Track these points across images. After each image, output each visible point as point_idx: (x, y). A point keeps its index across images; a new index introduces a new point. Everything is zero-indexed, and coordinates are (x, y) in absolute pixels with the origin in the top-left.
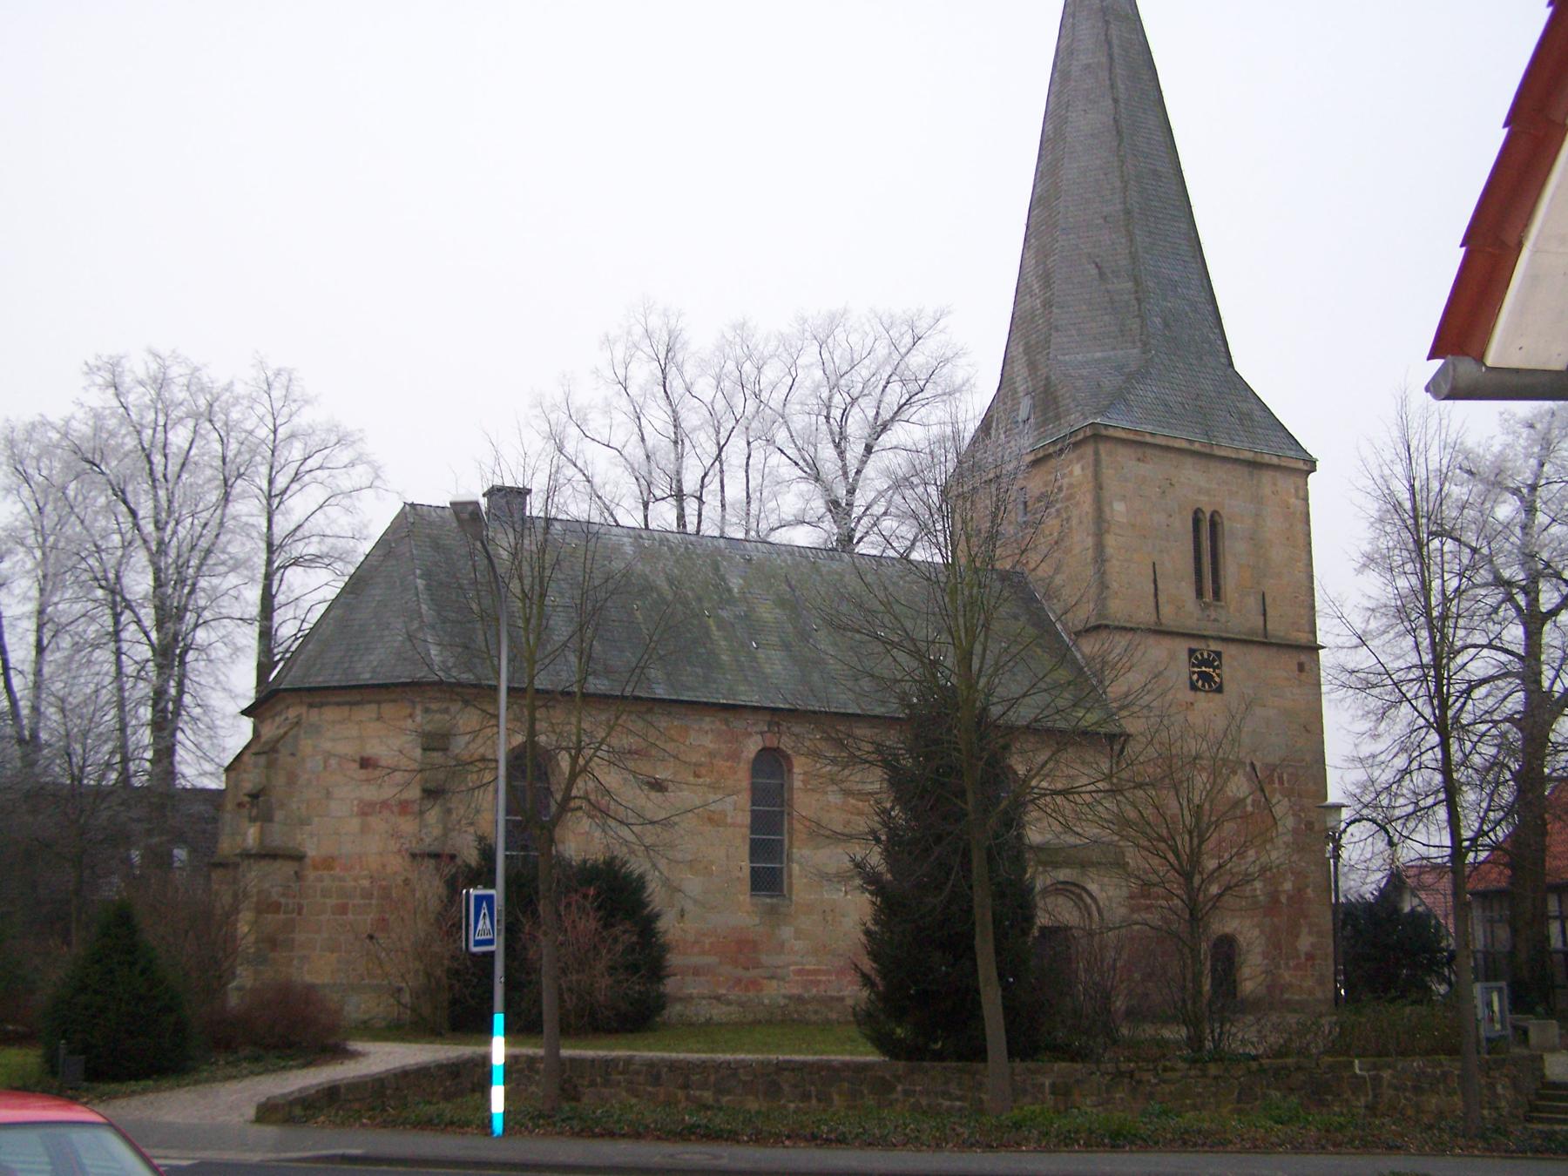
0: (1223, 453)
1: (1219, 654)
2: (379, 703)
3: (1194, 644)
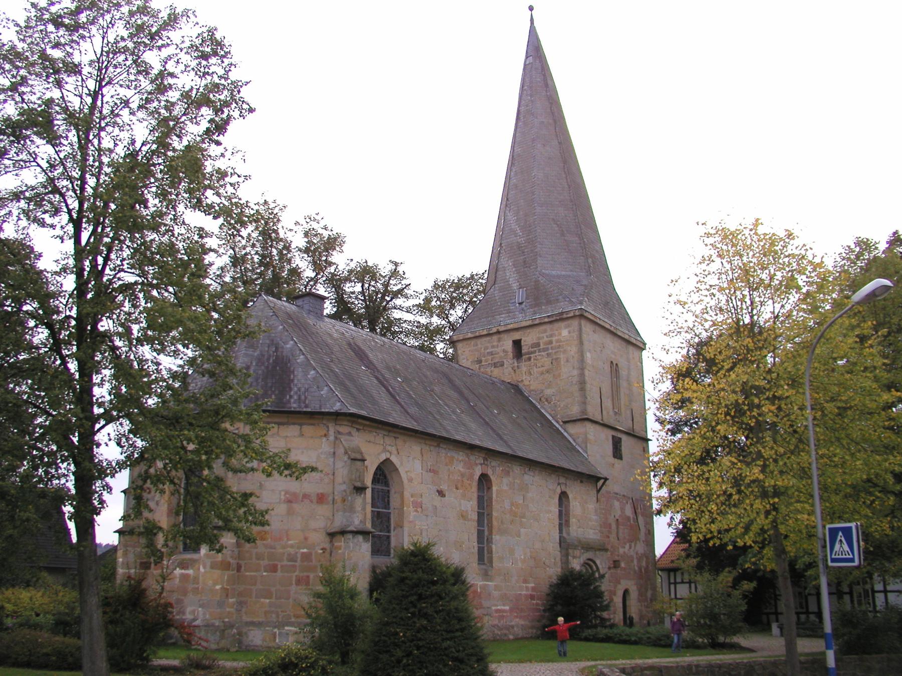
2: (301, 425)
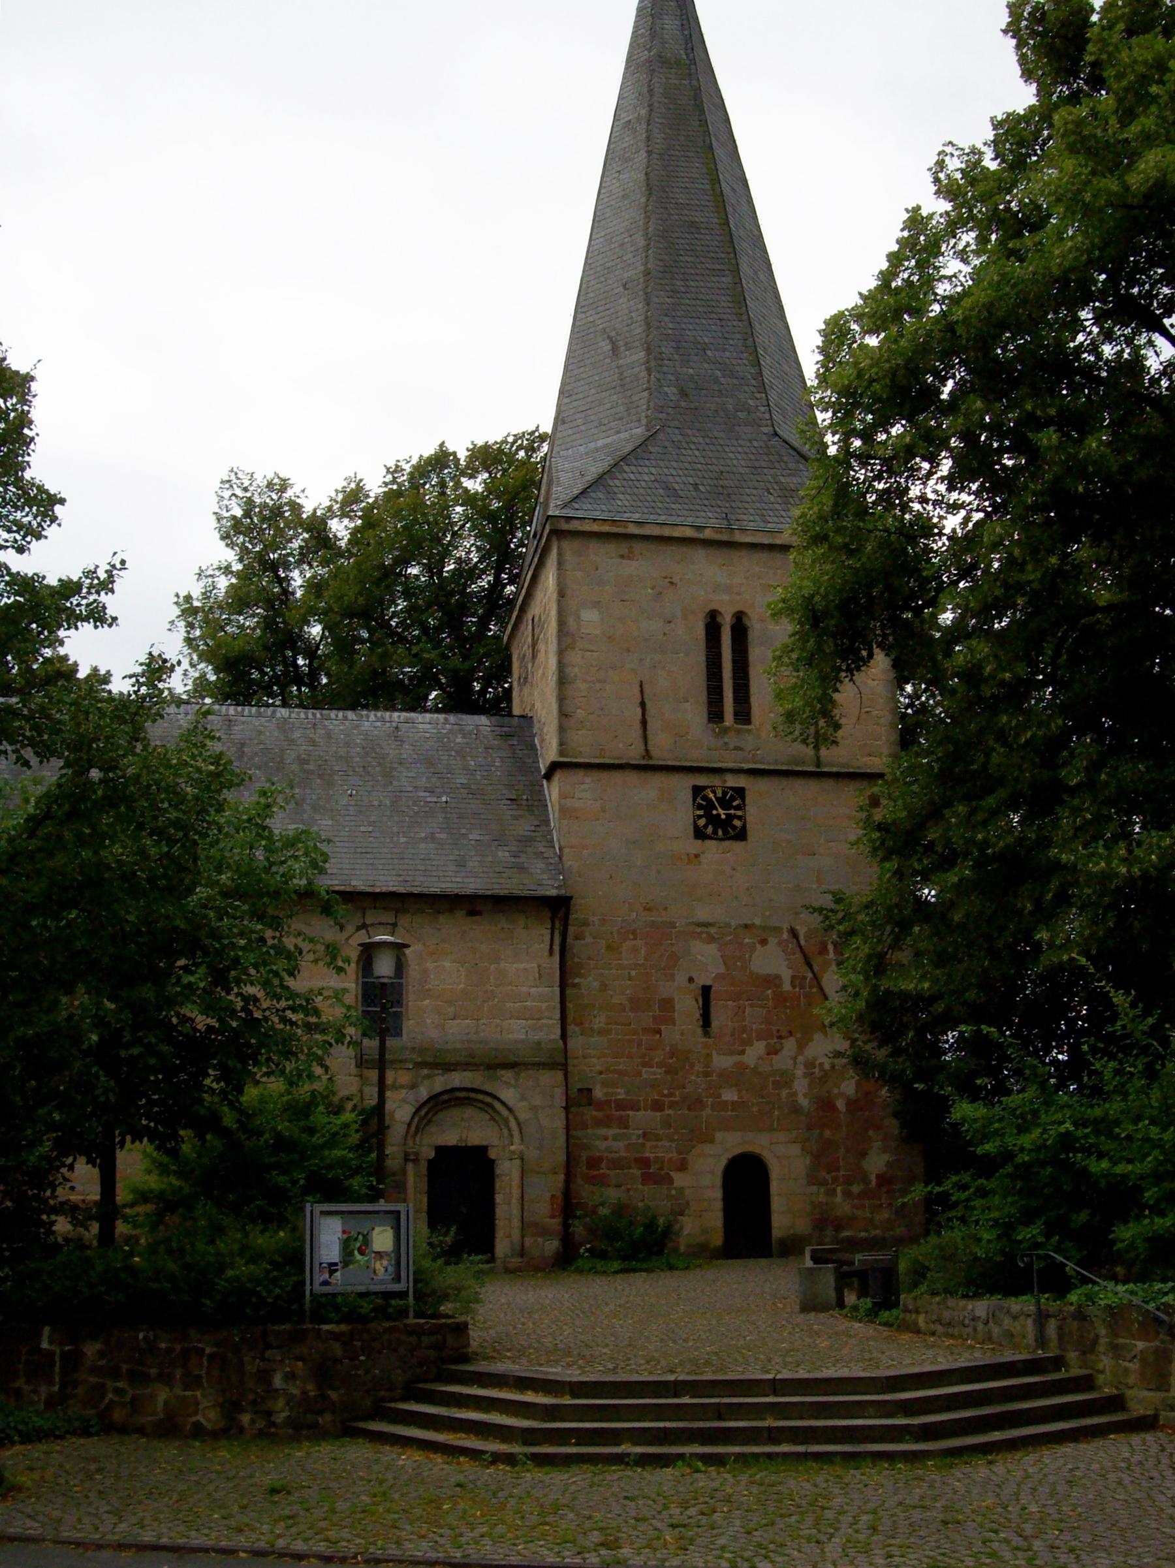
0: (748, 539)
1: (740, 792)
3: (702, 780)
